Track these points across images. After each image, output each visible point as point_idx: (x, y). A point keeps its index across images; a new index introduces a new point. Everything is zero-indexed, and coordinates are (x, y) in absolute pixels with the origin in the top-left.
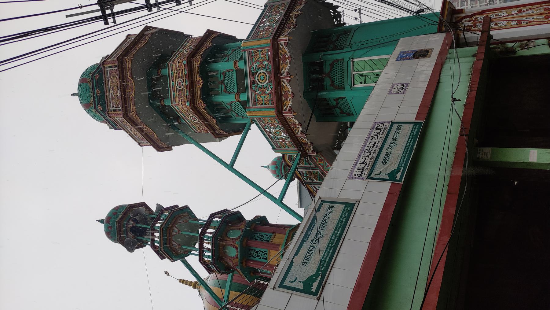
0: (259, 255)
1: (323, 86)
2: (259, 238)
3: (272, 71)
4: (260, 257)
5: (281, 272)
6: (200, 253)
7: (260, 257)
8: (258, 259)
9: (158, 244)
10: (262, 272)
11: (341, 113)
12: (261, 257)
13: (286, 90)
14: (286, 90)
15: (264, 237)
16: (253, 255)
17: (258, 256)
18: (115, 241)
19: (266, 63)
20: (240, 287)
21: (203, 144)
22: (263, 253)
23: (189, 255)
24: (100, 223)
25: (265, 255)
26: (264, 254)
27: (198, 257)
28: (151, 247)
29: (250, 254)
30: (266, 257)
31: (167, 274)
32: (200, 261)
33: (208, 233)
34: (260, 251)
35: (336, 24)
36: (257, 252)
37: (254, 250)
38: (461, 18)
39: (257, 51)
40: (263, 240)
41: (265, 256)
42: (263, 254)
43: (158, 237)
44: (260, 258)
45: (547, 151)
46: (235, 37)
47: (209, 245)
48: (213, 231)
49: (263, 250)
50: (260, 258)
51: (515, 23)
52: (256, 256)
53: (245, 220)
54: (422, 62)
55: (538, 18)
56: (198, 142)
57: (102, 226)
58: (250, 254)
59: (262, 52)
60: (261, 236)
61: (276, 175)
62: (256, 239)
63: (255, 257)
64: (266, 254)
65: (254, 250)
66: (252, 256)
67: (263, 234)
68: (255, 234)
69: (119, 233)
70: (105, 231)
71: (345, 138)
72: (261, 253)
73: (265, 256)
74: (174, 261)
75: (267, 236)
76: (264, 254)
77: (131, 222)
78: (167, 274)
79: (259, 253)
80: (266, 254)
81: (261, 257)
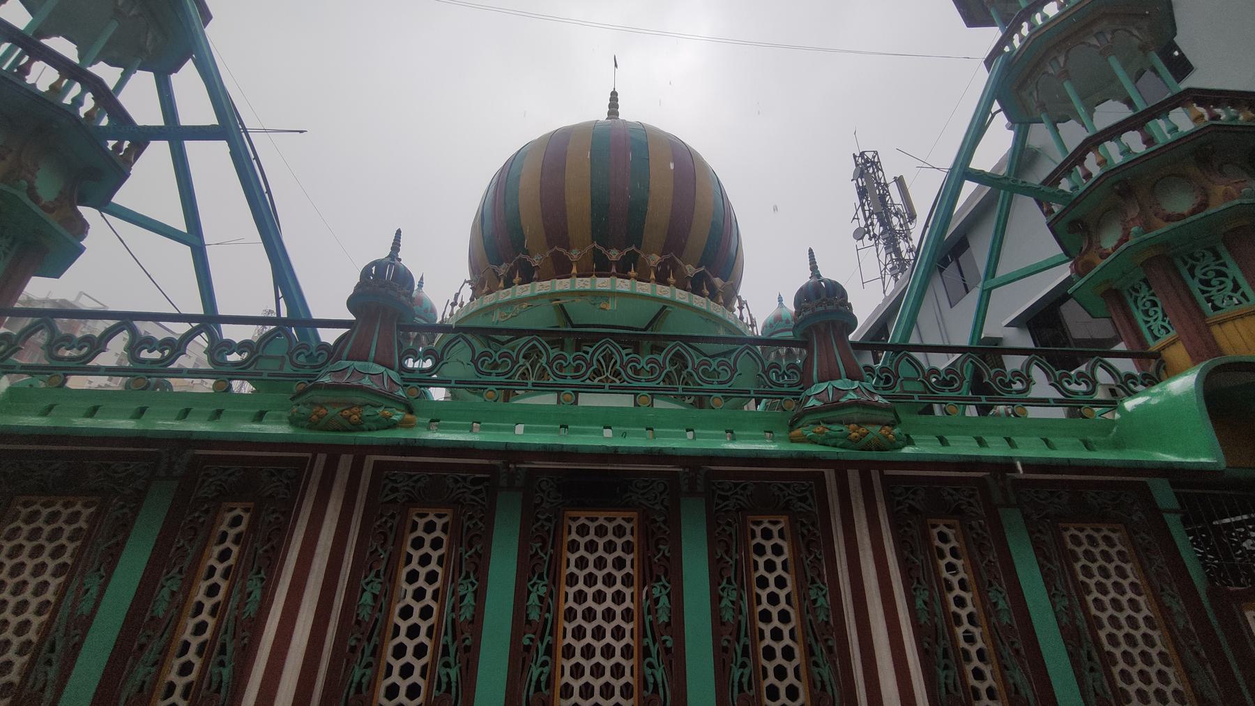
0: (1151, 313)
2: (1204, 274)
4: (1152, 298)
7: (1152, 298)
8: (1195, 286)
9: (1043, 20)
10: (1093, 357)
12: (1149, 322)
17: (1146, 313)
20: (1250, 468)
25: (1163, 331)
26: (1163, 327)
29: (1192, 256)
33: (82, 95)
38: (509, 396)
41: (1159, 330)
42: (1163, 324)
43: (1045, 17)
44: (1147, 322)
47: (48, 89)
48: (83, 111)
49: (1242, 281)
50: (1147, 322)
51: (365, 614)
53: (140, 69)
55: (379, 411)
58: (1192, 256)
63: (1138, 308)
71: (1176, 30)
73: (1159, 330)
76: (1163, 327)
79: (1144, 305)
81: (1149, 322)
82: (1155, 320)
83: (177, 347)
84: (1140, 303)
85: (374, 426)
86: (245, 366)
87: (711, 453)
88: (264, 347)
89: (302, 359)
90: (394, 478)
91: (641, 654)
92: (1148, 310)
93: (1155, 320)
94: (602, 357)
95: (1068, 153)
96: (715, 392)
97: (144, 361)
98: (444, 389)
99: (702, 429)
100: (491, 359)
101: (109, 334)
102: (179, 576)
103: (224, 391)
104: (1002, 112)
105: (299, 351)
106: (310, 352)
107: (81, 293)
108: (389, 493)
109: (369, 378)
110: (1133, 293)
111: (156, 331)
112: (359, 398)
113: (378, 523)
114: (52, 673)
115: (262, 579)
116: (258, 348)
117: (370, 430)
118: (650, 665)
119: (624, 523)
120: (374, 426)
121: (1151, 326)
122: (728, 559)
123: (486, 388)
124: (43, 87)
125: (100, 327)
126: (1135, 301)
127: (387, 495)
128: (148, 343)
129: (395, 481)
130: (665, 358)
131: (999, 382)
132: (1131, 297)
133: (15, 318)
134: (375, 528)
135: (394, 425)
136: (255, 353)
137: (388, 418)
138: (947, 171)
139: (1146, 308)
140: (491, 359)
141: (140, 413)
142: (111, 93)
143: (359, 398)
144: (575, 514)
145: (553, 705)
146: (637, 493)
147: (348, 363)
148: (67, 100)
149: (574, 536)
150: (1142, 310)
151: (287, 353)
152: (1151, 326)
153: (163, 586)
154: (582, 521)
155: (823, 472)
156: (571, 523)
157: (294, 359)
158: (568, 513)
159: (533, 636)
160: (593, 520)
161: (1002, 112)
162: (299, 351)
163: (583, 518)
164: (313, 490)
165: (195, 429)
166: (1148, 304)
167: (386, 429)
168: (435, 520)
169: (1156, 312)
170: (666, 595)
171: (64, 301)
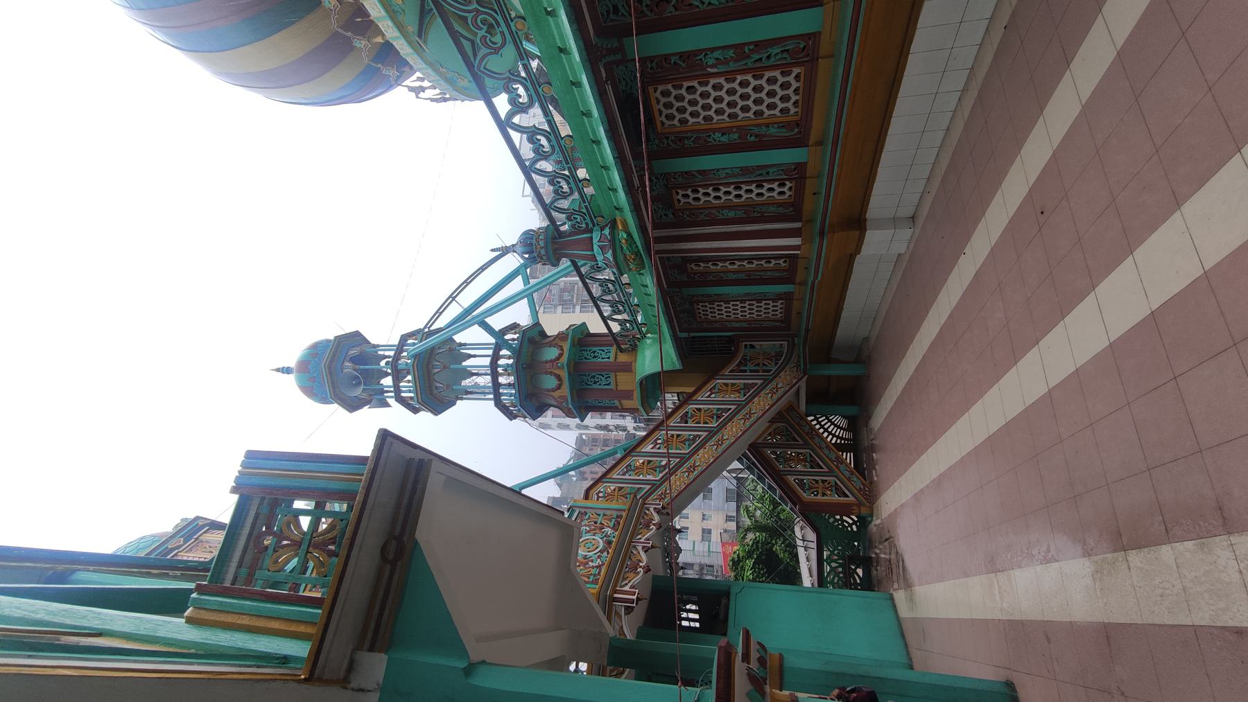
5: (718, 457)
6: (495, 396)
8: (595, 386)
18: (324, 400)
21: (403, 84)
22: (603, 376)
24: (280, 374)
25: (608, 379)
26: (606, 378)
27: (493, 402)
28: (396, 400)
31: (1042, 213)
32: (496, 405)
35: (569, 664)
44: (590, 350)
45: (182, 636)
50: (600, 385)
52: (598, 351)
54: (587, 424)
56: (539, 291)
57: (291, 379)
60: (594, 352)
61: (610, 172)
64: (609, 377)
66: (586, 383)
67: (595, 349)
68: (583, 350)
69: (334, 385)
70: (298, 386)
74: (440, 413)
75: (603, 351)
76: (606, 378)
77: (347, 364)
78: (1042, 213)
80: (609, 377)
83: (532, 133)
85: (634, 246)
86: (492, 12)
87: (598, 97)
88: (500, 74)
89: (498, 39)
90: (606, 13)
94: (477, 34)
96: (512, 31)
97: (530, 97)
98: (578, 172)
99: (554, 39)
100: (487, 36)
101: (542, 173)
102: (712, 136)
103: (525, 20)
105: (489, 43)
106: (487, 34)
107: (523, 196)
108: (620, 14)
109: (606, 254)
111: (527, 152)
112: (620, 257)
113: (649, 13)
114: (771, 171)
115: (706, 54)
116: (529, 132)
117: (637, 247)
118: (768, 57)
119: (659, 92)
120: (634, 246)
122: (693, 139)
123: (543, 95)
125: (516, 136)
126: (586, 359)
127: (623, 15)
128: (538, 151)
129: (608, 12)
130: (469, 11)
131: (481, 22)
133: (556, 220)
134: (655, 15)
135: (629, 235)
136: (510, 78)
137: (626, 240)
138: (512, 262)
140: (487, 36)
141: (606, 168)
143: (620, 257)
144: (659, 125)
146: (631, 86)
147: (595, 247)
148: (511, 361)
149: (676, 122)
151: (497, 54)
153: (719, 141)
154: (663, 118)
156: (666, 126)
157: (498, 45)
158: (659, 130)
159: (749, 135)
160: (661, 112)
162: (489, 43)
163: (661, 119)
165: (611, 156)
167: (633, 239)
168: (662, 103)
170: (712, 52)
171: (533, 201)
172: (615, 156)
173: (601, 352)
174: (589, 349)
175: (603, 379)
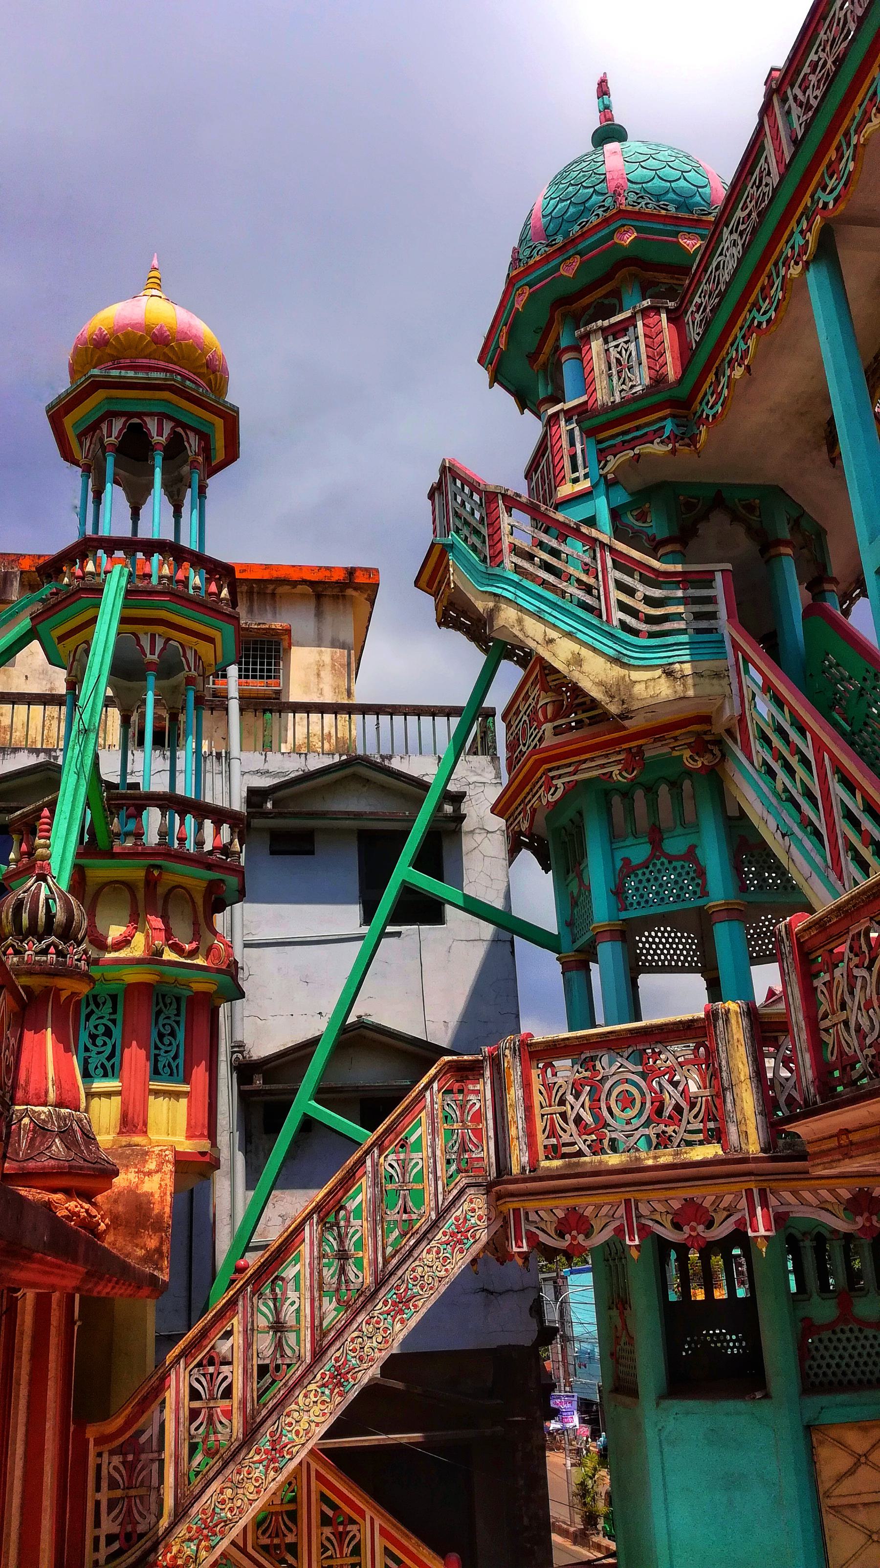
0: (99, 1042)
1: (623, 837)
2: (164, 1025)
3: (383, 1525)
4: (110, 1024)
7: (110, 1024)
11: (626, 861)
13: (555, 1080)
14: (555, 1080)
15: (169, 1048)
16: (94, 1017)
17: (93, 1037)
19: (541, 1065)
22: (109, 1059)
23: (546, 868)
26: (103, 1066)
30: (92, 1073)
34: (114, 1046)
36: (108, 1033)
37: (113, 1017)
39: (317, 1471)
40: (157, 1047)
41: (96, 1068)
42: (106, 1063)
46: (181, 517)
50: (157, 1047)
59: (561, 1122)
60: (173, 1034)
62: (159, 1013)
65: (113, 1017)
66: (92, 1012)
67: (181, 1035)
68: (178, 1009)
72: (108, 1050)
75: (175, 1057)
76: (103, 1066)
79: (105, 1044)
80: (164, 996)
81: (160, 1049)
82: (99, 1053)
84: (93, 1021)
91: (362, 1546)
92: (97, 1036)
93: (99, 1053)
95: (638, 1018)
104: (167, 789)
110: (161, 1005)
121: (159, 1055)
124: (767, 1065)
132: (87, 1007)
139: (170, 1038)
142: (157, 1396)
145: (672, 1566)
150: (175, 1040)
152: (159, 1055)
155: (372, 1130)
161: (167, 790)
164: (277, 1098)
166: (102, 1029)
169: (105, 1044)
172: (763, 1146)
173: (172, 1054)
174: (182, 1019)
175: (103, 1058)
